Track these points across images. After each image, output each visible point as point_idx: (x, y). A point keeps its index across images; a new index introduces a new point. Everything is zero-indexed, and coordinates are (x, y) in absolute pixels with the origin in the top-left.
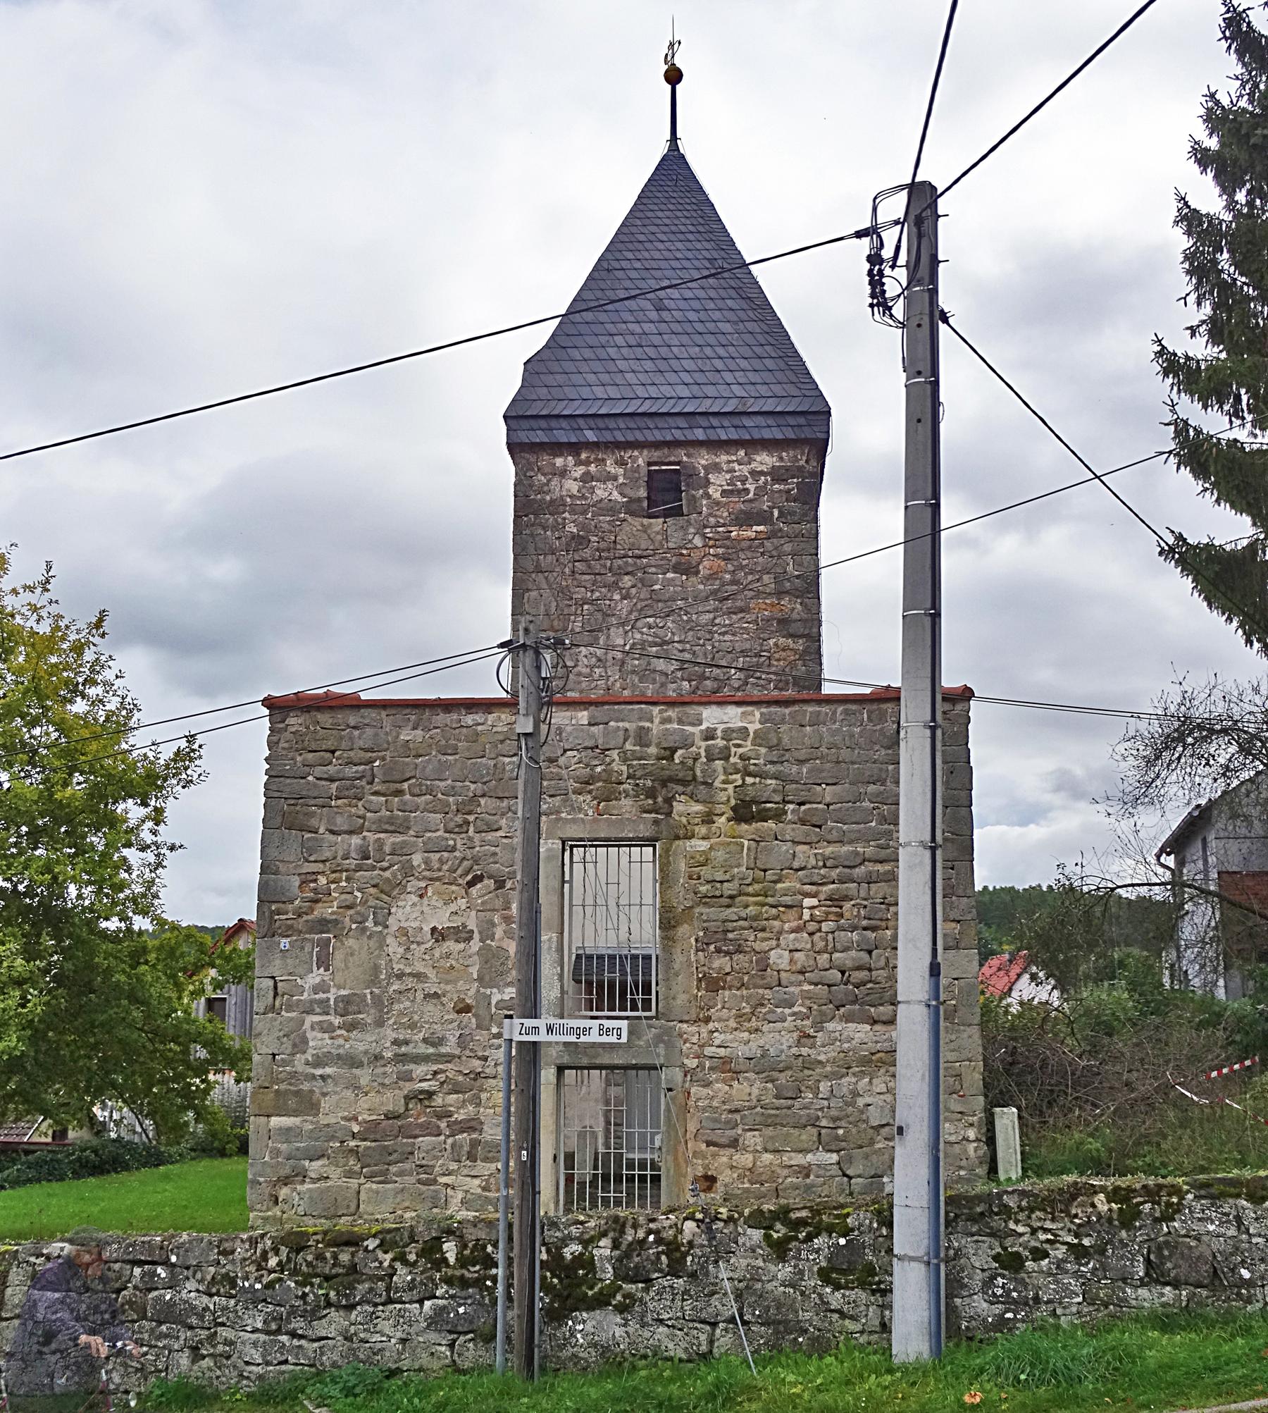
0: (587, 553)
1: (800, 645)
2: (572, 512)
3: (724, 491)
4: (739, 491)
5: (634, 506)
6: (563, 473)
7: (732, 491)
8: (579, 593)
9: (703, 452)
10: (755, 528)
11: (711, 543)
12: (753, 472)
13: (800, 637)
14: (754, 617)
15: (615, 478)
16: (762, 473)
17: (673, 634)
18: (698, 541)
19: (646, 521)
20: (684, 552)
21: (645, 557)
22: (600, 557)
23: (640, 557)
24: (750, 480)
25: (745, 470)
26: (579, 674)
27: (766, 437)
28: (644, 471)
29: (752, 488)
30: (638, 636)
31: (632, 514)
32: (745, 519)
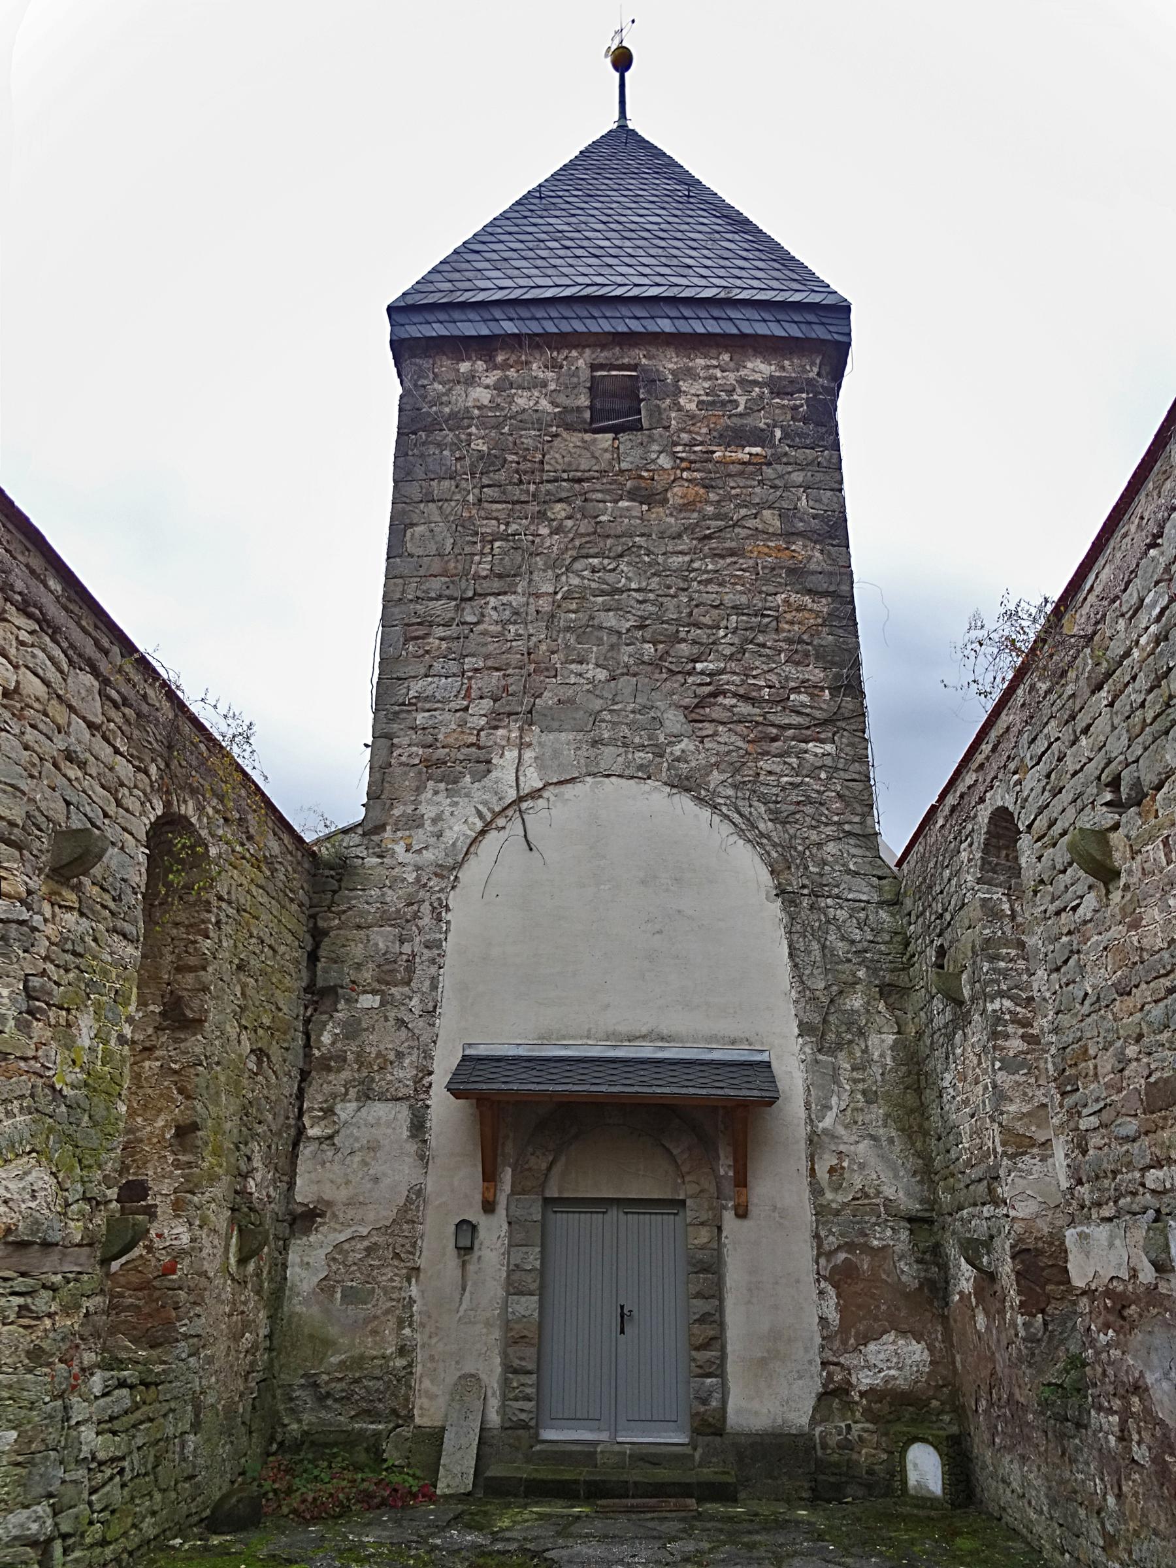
0: (502, 476)
1: (823, 605)
2: (482, 425)
3: (700, 402)
4: (723, 404)
5: (569, 418)
6: (470, 380)
7: (713, 403)
8: (489, 527)
9: (671, 353)
10: (747, 449)
11: (684, 465)
12: (742, 381)
13: (825, 594)
14: (751, 563)
15: (544, 384)
16: (755, 383)
17: (629, 579)
18: (665, 461)
19: (588, 437)
20: (645, 474)
21: (588, 480)
22: (521, 482)
23: (579, 481)
24: (739, 391)
25: (732, 377)
26: (484, 633)
27: (760, 332)
28: (585, 374)
29: (742, 401)
30: (576, 581)
31: (569, 428)
32: (737, 437)
